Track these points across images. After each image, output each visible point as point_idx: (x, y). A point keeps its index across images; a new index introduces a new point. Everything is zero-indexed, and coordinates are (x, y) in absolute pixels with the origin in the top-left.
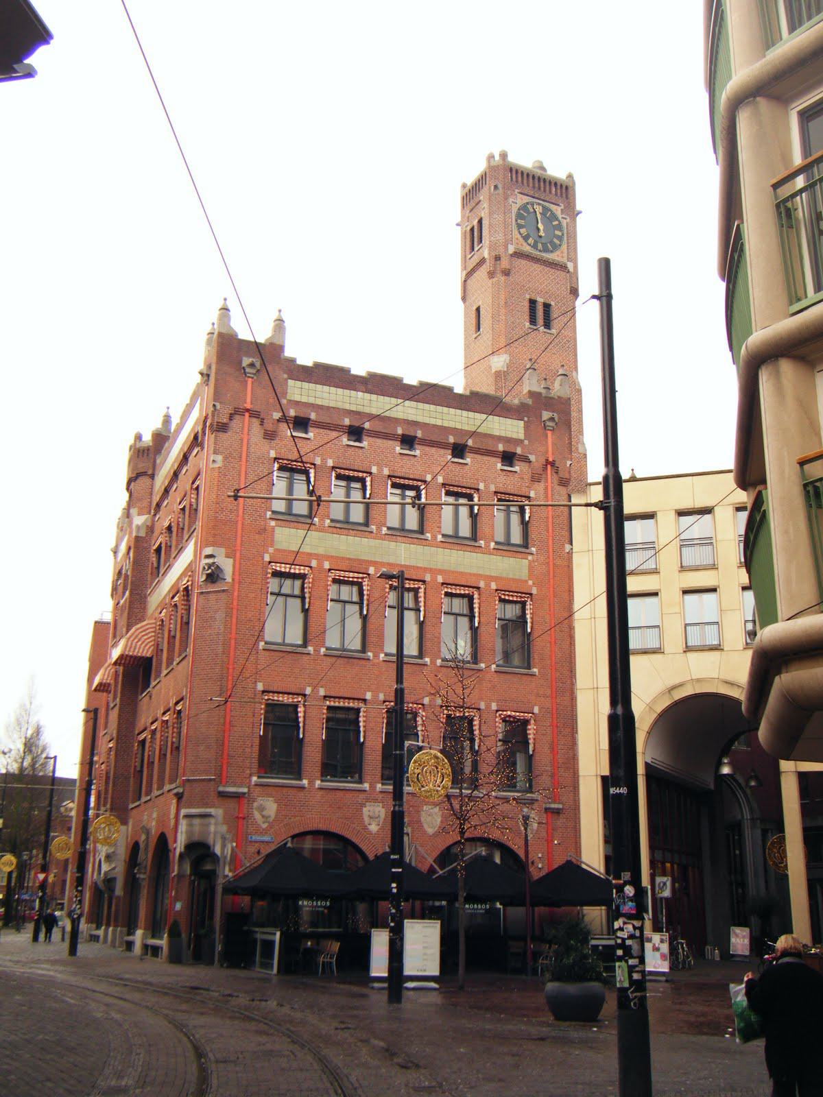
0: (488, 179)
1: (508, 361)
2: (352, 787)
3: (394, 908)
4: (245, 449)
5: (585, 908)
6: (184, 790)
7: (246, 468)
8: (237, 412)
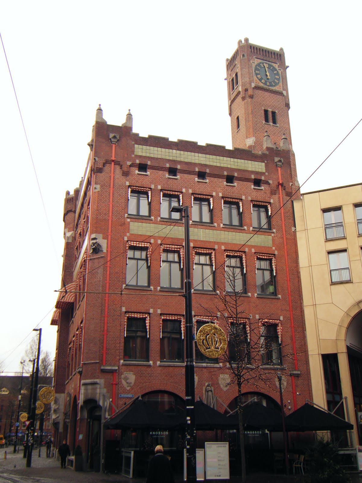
0: (239, 53)
1: (255, 140)
2: (178, 365)
3: (189, 435)
4: (112, 181)
5: (317, 432)
6: (82, 369)
7: (113, 191)
8: (107, 162)
